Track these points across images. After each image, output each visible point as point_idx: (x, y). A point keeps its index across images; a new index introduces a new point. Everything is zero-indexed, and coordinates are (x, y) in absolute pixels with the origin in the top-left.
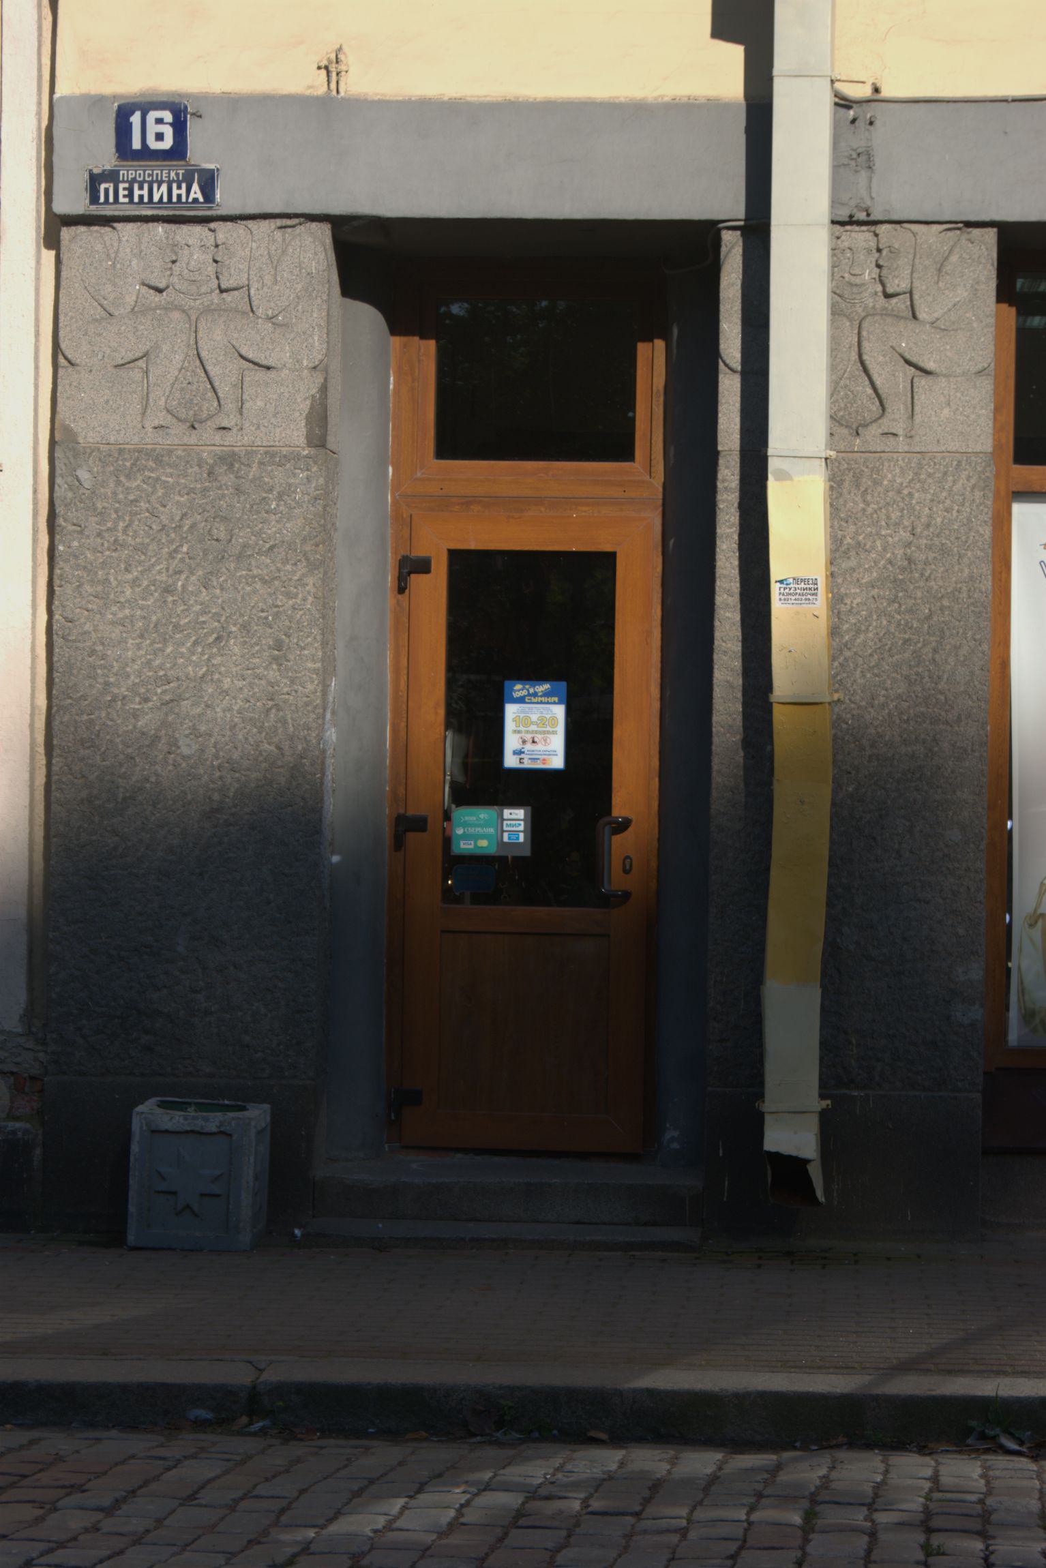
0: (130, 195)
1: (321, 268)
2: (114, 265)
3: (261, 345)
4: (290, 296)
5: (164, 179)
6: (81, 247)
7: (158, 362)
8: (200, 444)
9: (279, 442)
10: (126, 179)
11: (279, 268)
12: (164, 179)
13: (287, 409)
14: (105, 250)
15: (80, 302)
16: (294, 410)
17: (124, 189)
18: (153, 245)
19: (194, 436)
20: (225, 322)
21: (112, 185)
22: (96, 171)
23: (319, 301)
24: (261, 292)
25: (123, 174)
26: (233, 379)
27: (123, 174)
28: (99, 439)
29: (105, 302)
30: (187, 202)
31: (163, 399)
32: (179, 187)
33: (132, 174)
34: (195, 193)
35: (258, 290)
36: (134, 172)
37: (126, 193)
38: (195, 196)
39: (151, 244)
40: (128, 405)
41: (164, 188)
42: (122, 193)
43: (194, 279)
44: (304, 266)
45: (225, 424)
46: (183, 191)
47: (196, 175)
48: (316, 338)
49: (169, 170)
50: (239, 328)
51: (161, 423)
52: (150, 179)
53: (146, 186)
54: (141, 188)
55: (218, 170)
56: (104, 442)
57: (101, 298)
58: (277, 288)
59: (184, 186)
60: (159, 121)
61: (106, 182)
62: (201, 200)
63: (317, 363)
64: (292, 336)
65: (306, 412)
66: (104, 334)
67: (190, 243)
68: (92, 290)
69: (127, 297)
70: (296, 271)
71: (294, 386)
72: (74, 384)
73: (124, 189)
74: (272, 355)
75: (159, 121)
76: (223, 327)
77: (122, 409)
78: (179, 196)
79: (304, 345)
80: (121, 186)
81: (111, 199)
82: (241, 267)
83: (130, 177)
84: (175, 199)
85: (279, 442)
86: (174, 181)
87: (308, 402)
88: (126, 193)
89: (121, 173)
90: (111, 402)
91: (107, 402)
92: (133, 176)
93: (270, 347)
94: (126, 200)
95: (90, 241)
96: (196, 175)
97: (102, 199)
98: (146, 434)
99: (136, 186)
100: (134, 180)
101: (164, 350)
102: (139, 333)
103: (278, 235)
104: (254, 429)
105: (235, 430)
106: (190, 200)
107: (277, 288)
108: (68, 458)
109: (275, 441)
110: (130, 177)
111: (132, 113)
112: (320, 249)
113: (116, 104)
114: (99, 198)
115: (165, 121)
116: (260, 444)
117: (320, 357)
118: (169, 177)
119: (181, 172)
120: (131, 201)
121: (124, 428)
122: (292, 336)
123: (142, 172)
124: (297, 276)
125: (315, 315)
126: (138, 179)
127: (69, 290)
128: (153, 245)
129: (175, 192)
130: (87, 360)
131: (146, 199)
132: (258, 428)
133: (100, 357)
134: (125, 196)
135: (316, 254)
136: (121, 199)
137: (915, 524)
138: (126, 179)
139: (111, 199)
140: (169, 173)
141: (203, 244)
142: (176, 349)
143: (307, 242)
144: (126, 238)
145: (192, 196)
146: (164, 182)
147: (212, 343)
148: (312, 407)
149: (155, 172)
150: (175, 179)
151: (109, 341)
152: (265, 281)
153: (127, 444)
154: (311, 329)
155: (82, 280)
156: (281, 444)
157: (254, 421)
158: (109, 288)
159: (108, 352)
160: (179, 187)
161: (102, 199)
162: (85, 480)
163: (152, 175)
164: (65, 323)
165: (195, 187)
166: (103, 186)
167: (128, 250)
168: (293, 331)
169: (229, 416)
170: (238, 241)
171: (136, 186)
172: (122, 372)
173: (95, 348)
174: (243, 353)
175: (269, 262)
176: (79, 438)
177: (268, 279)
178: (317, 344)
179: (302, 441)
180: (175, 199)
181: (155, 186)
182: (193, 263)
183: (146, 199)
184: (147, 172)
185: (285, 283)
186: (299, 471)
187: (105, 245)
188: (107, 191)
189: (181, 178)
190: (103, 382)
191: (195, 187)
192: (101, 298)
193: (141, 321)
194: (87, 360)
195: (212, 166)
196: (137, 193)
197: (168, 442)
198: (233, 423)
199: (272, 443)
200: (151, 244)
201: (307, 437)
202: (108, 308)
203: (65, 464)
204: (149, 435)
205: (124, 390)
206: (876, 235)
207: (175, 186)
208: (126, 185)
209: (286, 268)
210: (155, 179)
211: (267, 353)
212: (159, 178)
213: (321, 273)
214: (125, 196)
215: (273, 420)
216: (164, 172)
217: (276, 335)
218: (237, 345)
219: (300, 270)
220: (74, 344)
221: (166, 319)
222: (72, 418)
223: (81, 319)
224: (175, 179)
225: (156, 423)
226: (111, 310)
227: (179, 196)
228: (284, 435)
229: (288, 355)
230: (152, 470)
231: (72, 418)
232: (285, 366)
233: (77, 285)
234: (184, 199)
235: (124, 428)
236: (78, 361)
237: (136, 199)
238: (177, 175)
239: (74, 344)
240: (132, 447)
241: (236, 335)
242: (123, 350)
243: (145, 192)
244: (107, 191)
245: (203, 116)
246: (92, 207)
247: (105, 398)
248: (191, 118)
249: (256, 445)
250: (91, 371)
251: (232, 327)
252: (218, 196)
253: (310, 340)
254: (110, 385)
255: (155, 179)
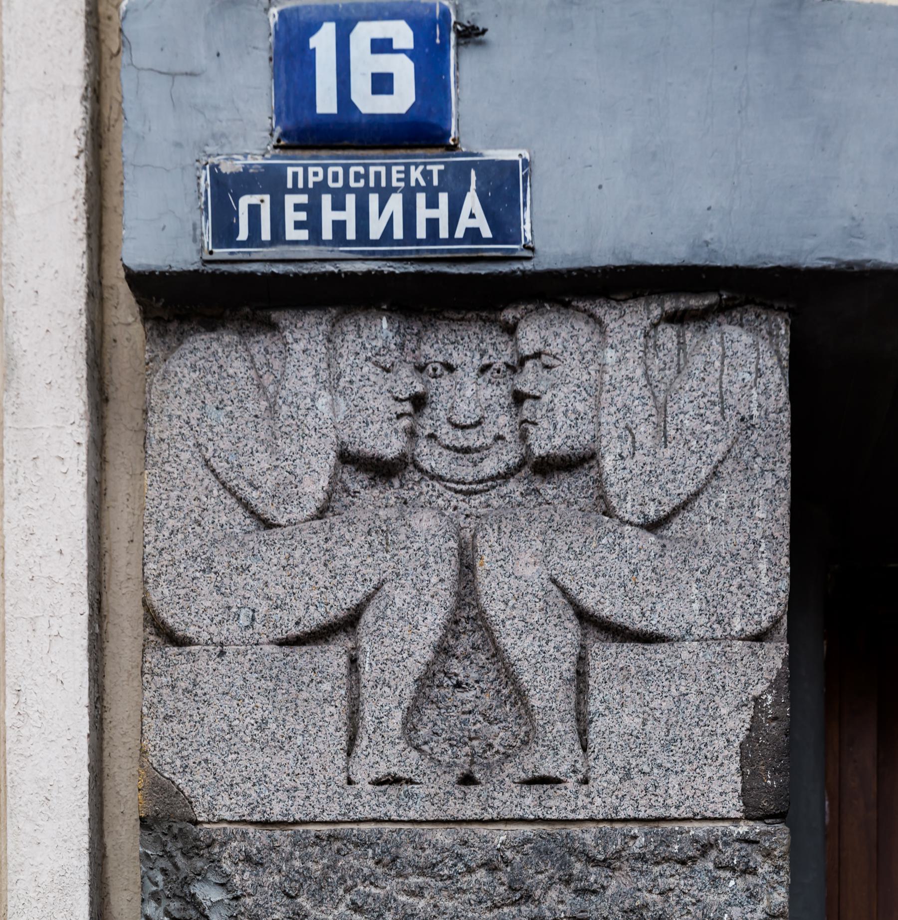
0: (313, 224)
1: (771, 405)
2: (272, 409)
3: (630, 586)
4: (698, 470)
5: (395, 184)
6: (194, 368)
7: (385, 630)
8: (487, 817)
9: (677, 807)
10: (301, 185)
11: (672, 409)
12: (395, 184)
13: (697, 730)
14: (252, 373)
15: (194, 494)
16: (713, 733)
17: (298, 207)
18: (368, 359)
19: (472, 799)
20: (542, 533)
21: (267, 198)
22: (226, 168)
23: (770, 482)
24: (629, 463)
25: (295, 175)
26: (566, 666)
27: (295, 175)
28: (245, 811)
29: (255, 494)
30: (451, 240)
31: (398, 715)
32: (432, 203)
33: (316, 174)
34: (472, 216)
35: (622, 458)
36: (320, 170)
37: (302, 216)
38: (472, 224)
39: (363, 356)
40: (313, 731)
41: (396, 203)
42: (291, 216)
43: (466, 444)
44: (731, 401)
45: (548, 768)
46: (442, 213)
47: (473, 173)
48: (763, 566)
49: (407, 166)
50: (576, 547)
51: (394, 770)
52: (362, 183)
53: (351, 200)
54: (338, 205)
55: (526, 163)
56: (256, 817)
57: (243, 484)
58: (668, 452)
59: (443, 198)
60: (381, 46)
61: (252, 192)
62: (487, 233)
63: (765, 624)
64: (705, 563)
65: (742, 737)
66: (253, 569)
67: (455, 360)
68: (221, 467)
69: (307, 480)
70: (713, 415)
71: (710, 678)
72: (182, 685)
73: (298, 207)
74: (659, 607)
75: (381, 46)
76: (540, 546)
77: (299, 740)
78: (432, 224)
79: (736, 582)
80: (290, 200)
81: (266, 235)
82: (580, 407)
83: (312, 180)
84: (421, 232)
85: (677, 807)
86: (419, 189)
87: (746, 715)
88: (302, 216)
89: (290, 171)
90: (273, 726)
91: (262, 725)
92: (320, 178)
93: (653, 589)
94: (304, 235)
95: (214, 354)
96: (473, 173)
97: (243, 234)
98: (358, 796)
99: (326, 200)
100: (322, 187)
101: (399, 602)
102: (338, 563)
103: (668, 335)
104: (616, 778)
105: (571, 784)
106: (459, 233)
107: (668, 452)
108: (171, 857)
109: (666, 806)
110: (312, 180)
111: (313, 28)
112: (769, 361)
113: (274, 11)
114: (236, 230)
115: (396, 46)
116: (631, 813)
117: (773, 610)
118: (407, 179)
119: (435, 169)
120: (316, 237)
121: (306, 785)
122: (705, 563)
123: (340, 170)
124: (716, 423)
125: (759, 514)
126: (331, 184)
127: (167, 467)
128: (368, 359)
129: (423, 214)
130: (213, 629)
131: (351, 234)
132: (628, 776)
133: (244, 621)
134: (298, 225)
135: (759, 373)
136: (292, 234)
137: (516, 781)
138: (301, 185)
139: (266, 235)
140: (407, 172)
141: (486, 361)
142: (427, 598)
143: (737, 346)
144: (302, 345)
145: (464, 222)
146: (395, 190)
147: (514, 583)
148: (755, 726)
149: (372, 170)
150: (423, 183)
151: (266, 584)
152: (638, 438)
153: (313, 822)
154: (751, 546)
155: (198, 445)
156: (683, 812)
157: (618, 763)
158: (263, 460)
159: (263, 609)
160: (432, 203)
161: (243, 234)
162: (214, 904)
163: (366, 176)
164: (160, 545)
165: (472, 202)
166: (245, 202)
167: (308, 372)
168: (708, 552)
169: (555, 750)
170: (571, 346)
171: (326, 200)
172: (301, 656)
173: (231, 601)
174: (589, 600)
175: (646, 392)
176: (197, 810)
177: (644, 433)
178: (765, 580)
179: (733, 806)
180: (421, 232)
181: (374, 200)
182: (463, 406)
183: (351, 234)
184: (352, 170)
185: (687, 442)
186: (728, 874)
187: (252, 361)
188: (254, 211)
189: (436, 182)
190: (252, 678)
191: (472, 202)
192: (243, 484)
193: (342, 537)
194: (213, 629)
195: (510, 155)
196: (328, 216)
197: (412, 815)
198: (564, 768)
199: (661, 812)
200: (363, 356)
201: (745, 794)
202: (261, 508)
203: (164, 871)
204: (366, 798)
205: (304, 695)
206: (760, 637)
207: (421, 198)
208: (303, 199)
209: (688, 407)
210: (372, 184)
211: (647, 604)
212: (383, 184)
213: (772, 416)
214: (298, 225)
215: (662, 758)
216: (394, 169)
217: (667, 560)
218: (573, 587)
219: (722, 412)
220: (182, 592)
221: (403, 530)
222: (178, 763)
223: (196, 535)
224: (423, 183)
225: (383, 770)
226: (269, 511)
227: (432, 224)
228: (689, 792)
229: (696, 606)
230: (371, 880)
231: (178, 763)
232: (688, 632)
233: (185, 456)
234: (444, 233)
235: (306, 785)
236: (191, 632)
237: (327, 233)
238: (427, 175)
239: (182, 592)
240: (325, 829)
241: (572, 564)
242: (300, 605)
243: (349, 215)
244: (254, 211)
245: (486, 27)
246: (222, 253)
247: (259, 715)
248: (458, 45)
249: (622, 815)
250: (222, 653)
251: (560, 544)
252: (526, 227)
253: (750, 574)
254: (271, 685)
255: (372, 184)
